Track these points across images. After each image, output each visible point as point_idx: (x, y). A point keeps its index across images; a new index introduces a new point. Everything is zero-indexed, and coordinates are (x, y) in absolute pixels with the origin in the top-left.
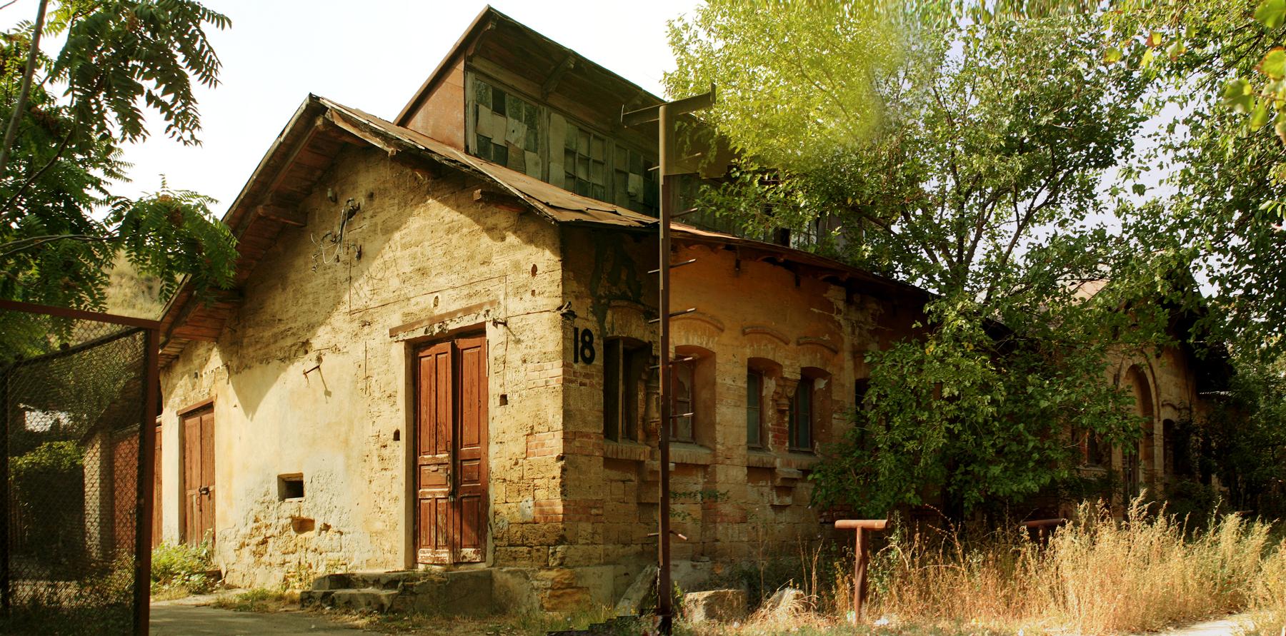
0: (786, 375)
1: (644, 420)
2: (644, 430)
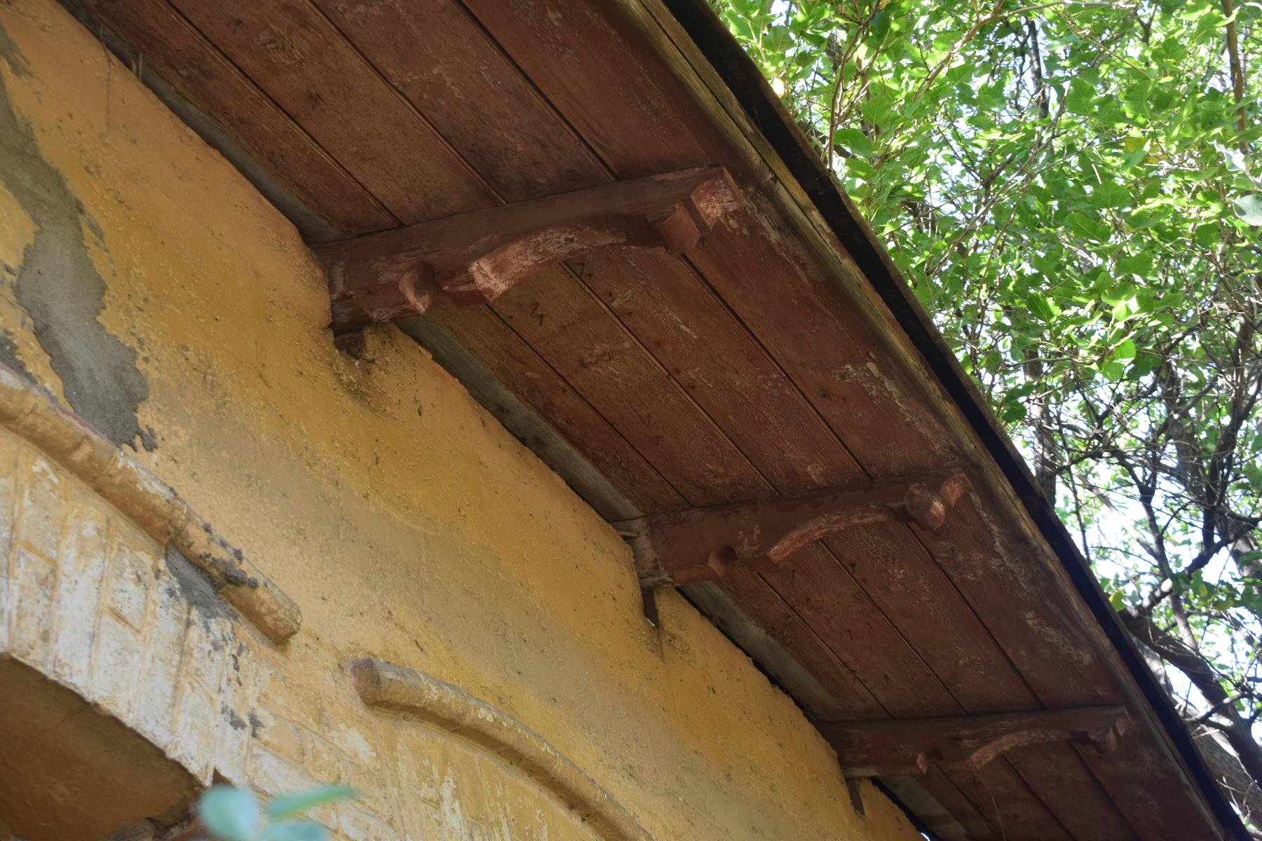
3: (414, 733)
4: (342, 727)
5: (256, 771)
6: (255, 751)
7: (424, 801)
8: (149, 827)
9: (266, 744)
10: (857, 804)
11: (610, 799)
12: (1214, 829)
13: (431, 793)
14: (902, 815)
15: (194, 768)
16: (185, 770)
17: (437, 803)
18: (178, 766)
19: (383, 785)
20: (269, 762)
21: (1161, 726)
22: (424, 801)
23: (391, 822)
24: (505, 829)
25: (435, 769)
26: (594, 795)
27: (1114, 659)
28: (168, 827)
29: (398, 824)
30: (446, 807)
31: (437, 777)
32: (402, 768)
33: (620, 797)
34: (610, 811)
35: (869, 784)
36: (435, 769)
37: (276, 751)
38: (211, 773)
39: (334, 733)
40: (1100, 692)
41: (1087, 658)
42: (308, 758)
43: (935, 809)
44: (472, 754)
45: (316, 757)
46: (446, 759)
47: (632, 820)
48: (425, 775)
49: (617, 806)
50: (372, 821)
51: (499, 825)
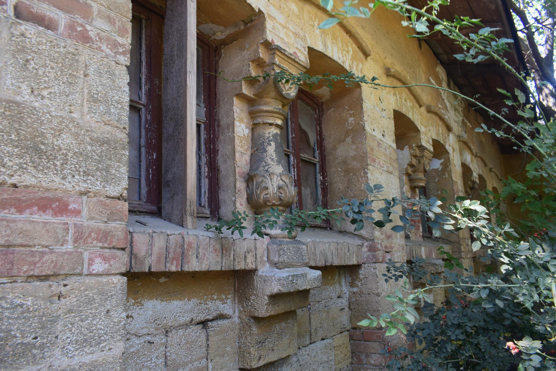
0: (424, 144)
1: (249, 179)
2: (250, 200)
3: (308, 7)
4: (291, 2)
5: (269, 10)
6: (269, 5)
7: (310, 25)
8: (243, 23)
9: (271, 3)
10: (420, 46)
11: (357, 32)
12: (517, 61)
13: (312, 23)
14: (431, 51)
15: (254, 6)
16: (251, 6)
17: (313, 26)
18: (250, 5)
19: (300, 19)
20: (272, 8)
21: (509, 30)
22: (310, 25)
23: (302, 29)
24: (330, 36)
25: (313, 18)
26: (353, 30)
27: (501, 8)
28: (247, 24)
29: (303, 29)
30: (316, 27)
31: (314, 19)
32: (305, 16)
33: (359, 32)
34: (357, 35)
35: (424, 41)
36: (313, 18)
37: (274, 6)
38: (258, 8)
39: (288, 4)
40: (495, 18)
41: (493, 7)
42: (282, 9)
43: (440, 51)
44: (323, 15)
45: (284, 9)
46: (316, 16)
47: (362, 38)
48: (311, 18)
49: (359, 34)
50: (297, 28)
51: (329, 35)
